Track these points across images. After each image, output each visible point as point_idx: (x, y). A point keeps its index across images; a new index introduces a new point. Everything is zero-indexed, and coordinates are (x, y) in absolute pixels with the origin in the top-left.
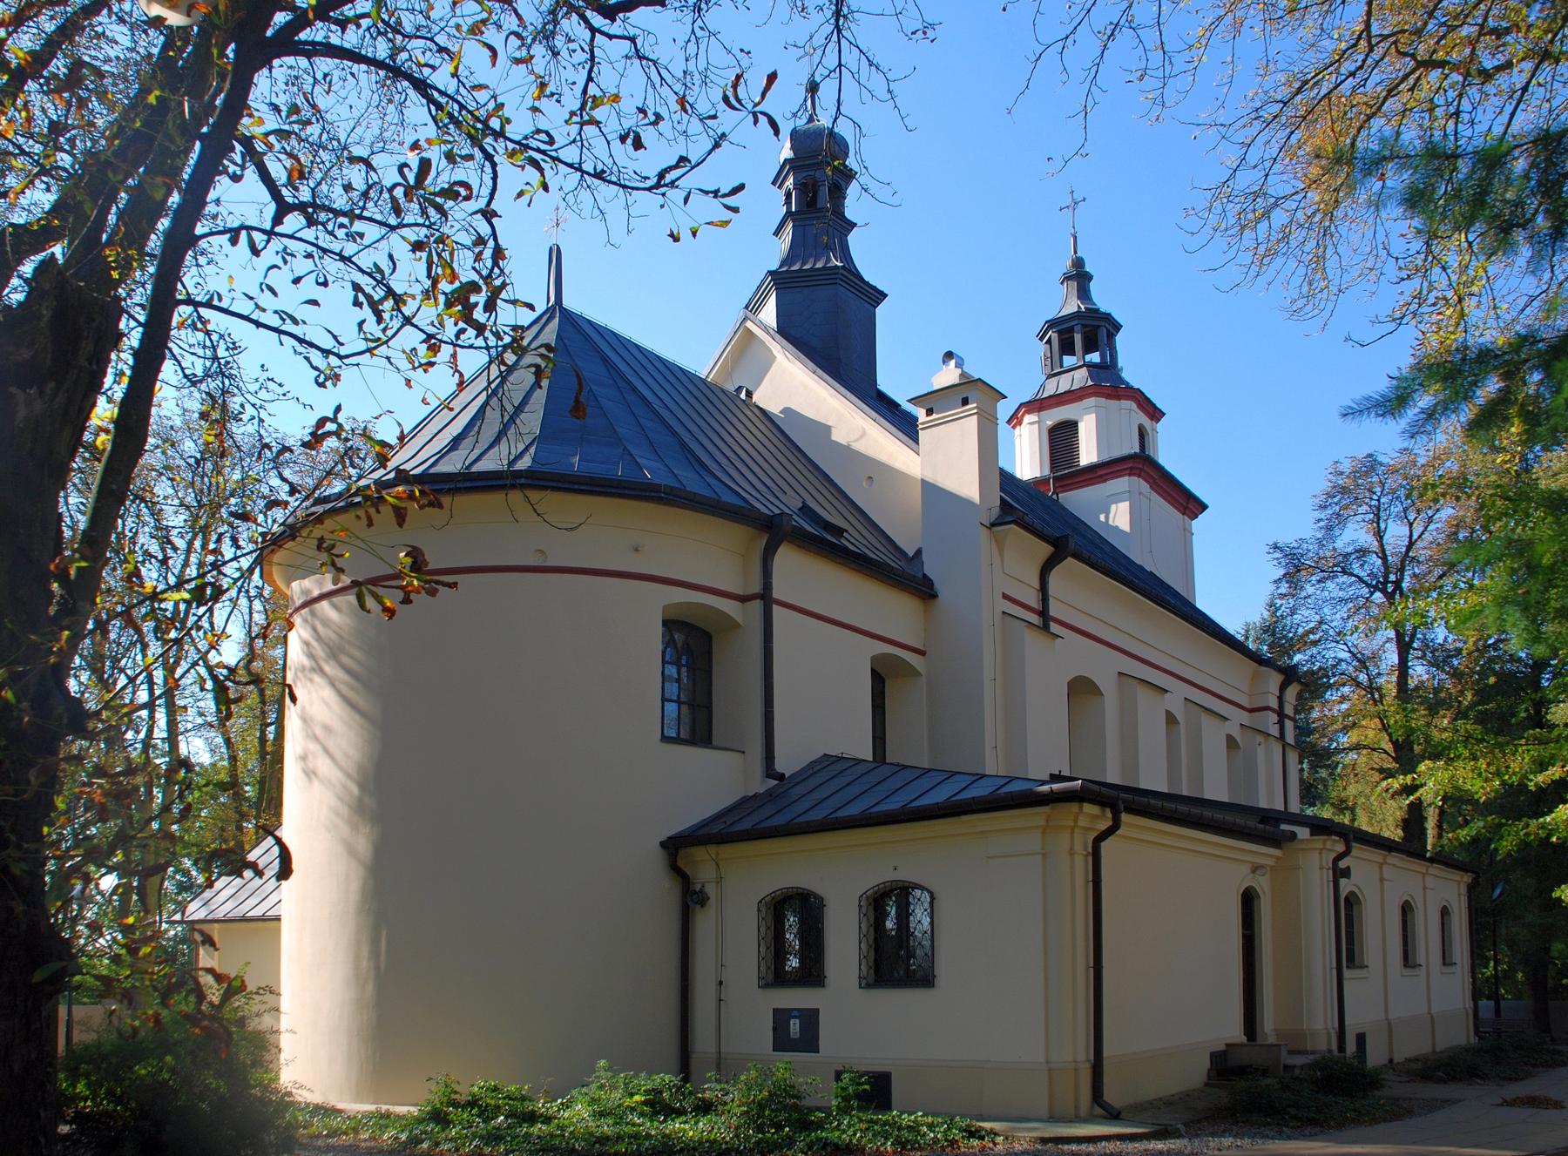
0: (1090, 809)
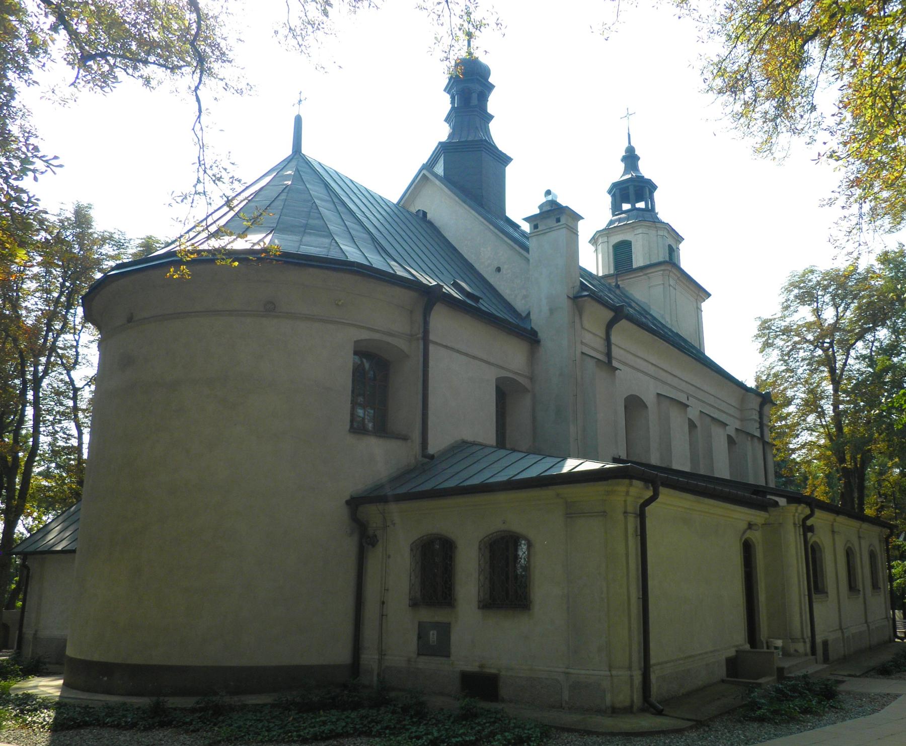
0: (637, 483)
